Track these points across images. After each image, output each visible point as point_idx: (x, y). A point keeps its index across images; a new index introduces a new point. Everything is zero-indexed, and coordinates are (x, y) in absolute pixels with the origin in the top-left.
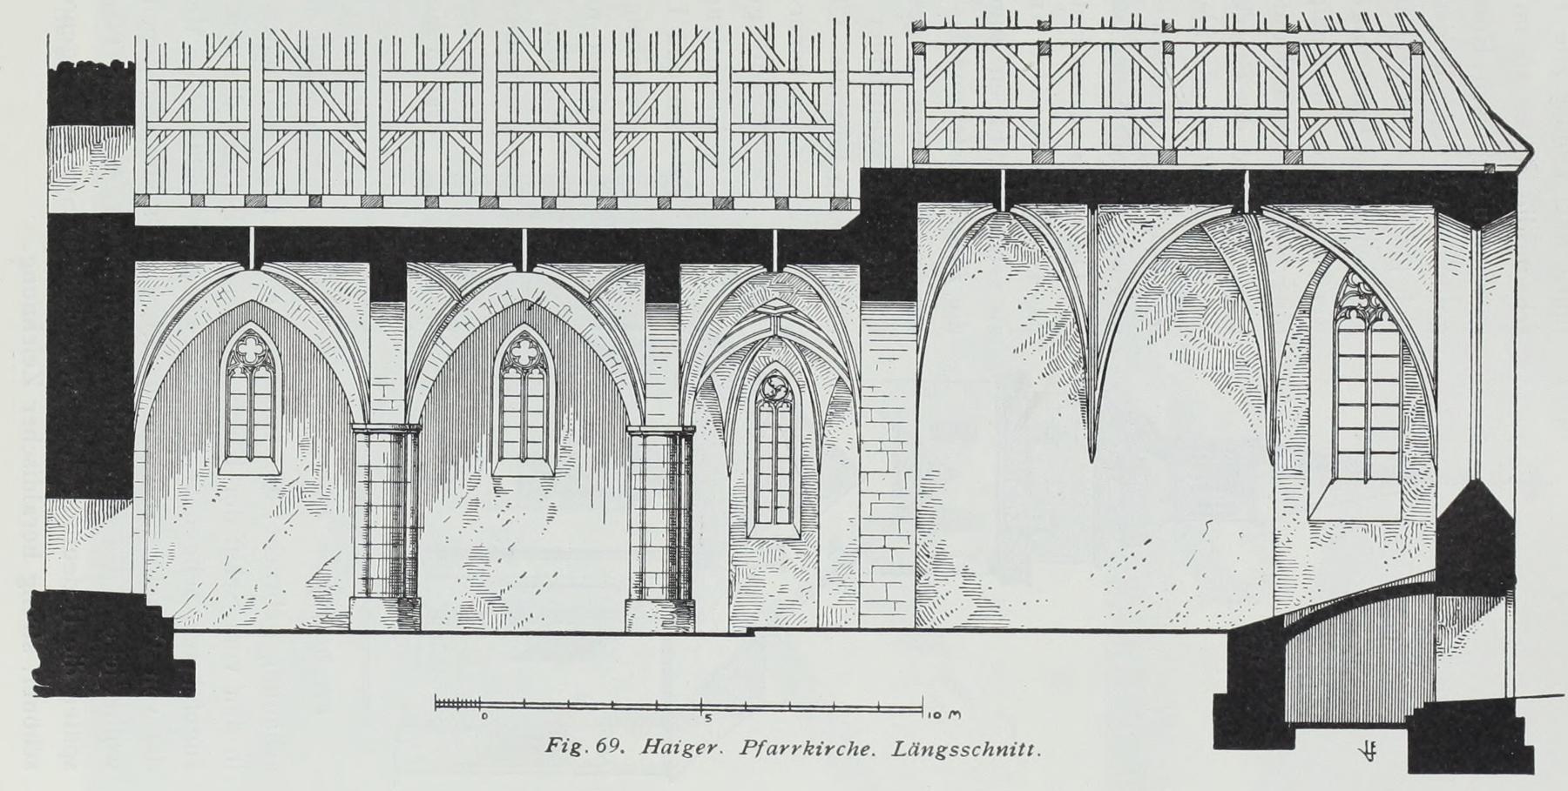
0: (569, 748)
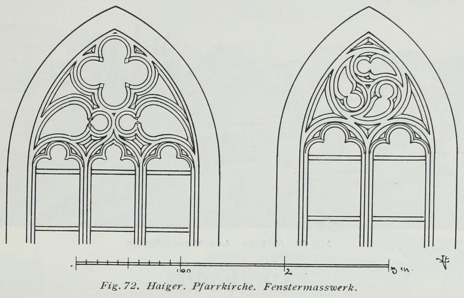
0: (112, 287)
